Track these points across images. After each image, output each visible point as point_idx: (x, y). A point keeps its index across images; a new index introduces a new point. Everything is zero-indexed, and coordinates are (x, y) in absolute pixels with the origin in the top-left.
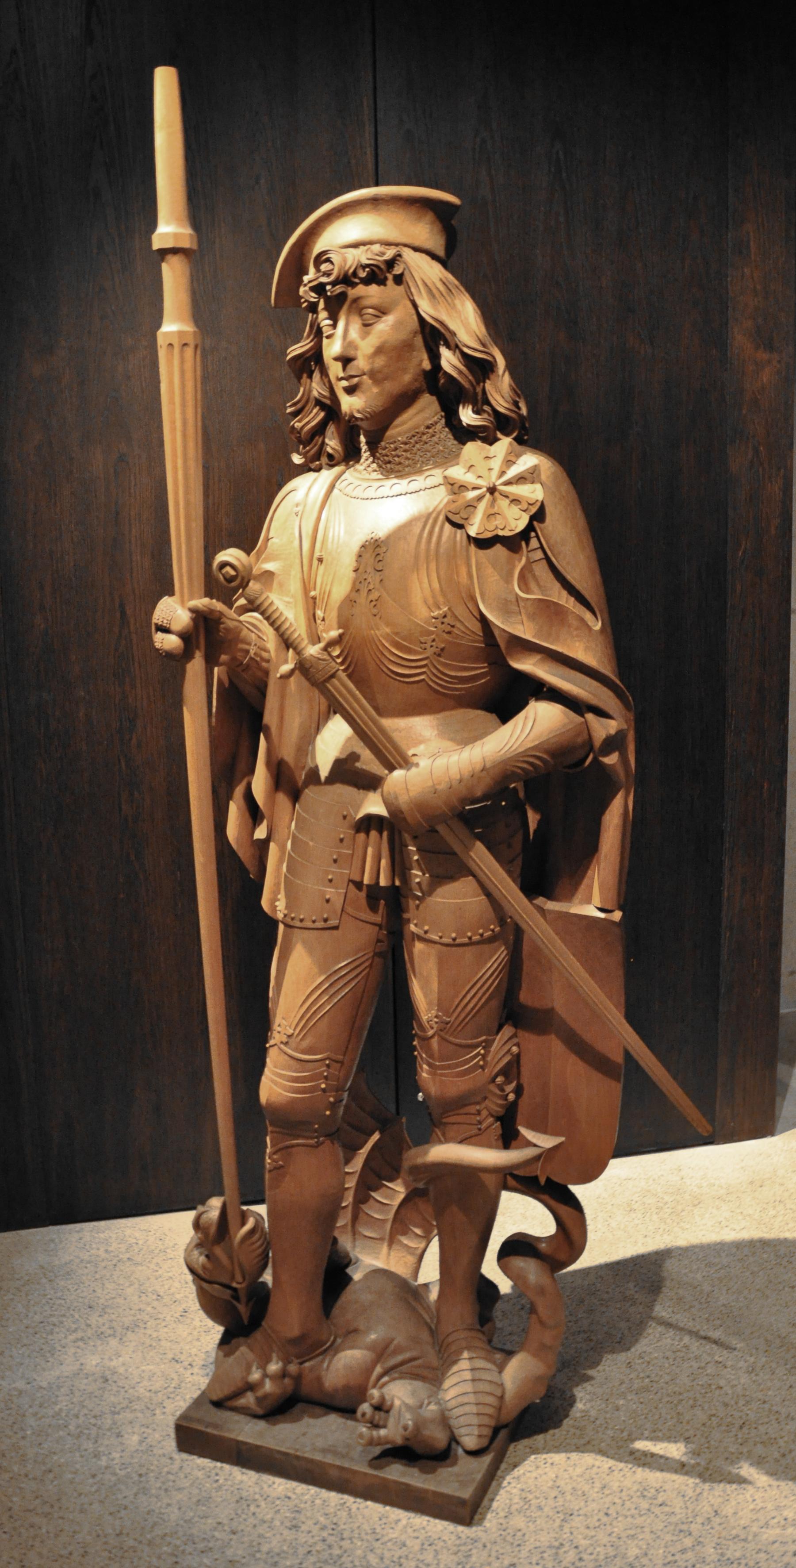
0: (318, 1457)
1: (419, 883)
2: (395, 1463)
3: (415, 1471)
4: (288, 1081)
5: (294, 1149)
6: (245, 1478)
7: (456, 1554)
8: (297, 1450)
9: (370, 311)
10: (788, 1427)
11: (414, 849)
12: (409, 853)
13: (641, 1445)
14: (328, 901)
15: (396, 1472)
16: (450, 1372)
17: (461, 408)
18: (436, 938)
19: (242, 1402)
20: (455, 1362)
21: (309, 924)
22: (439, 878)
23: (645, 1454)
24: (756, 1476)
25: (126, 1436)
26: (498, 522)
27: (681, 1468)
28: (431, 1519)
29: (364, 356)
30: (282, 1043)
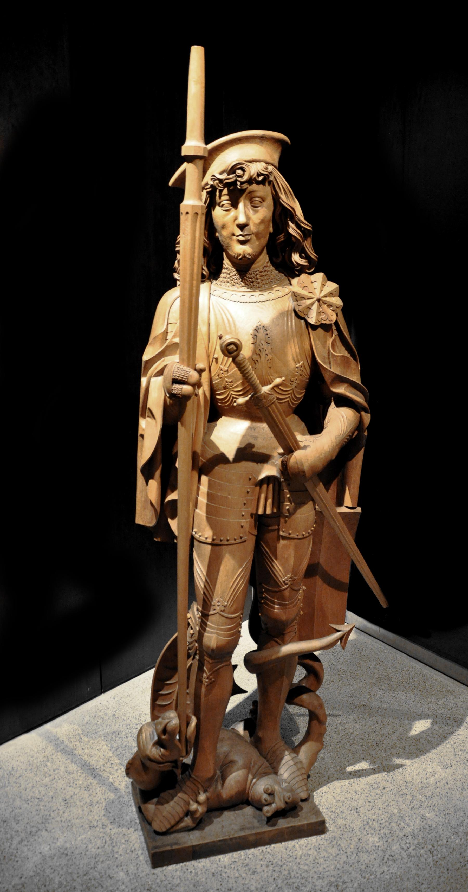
0: (242, 834)
1: (288, 510)
2: (279, 819)
3: (289, 819)
4: (225, 632)
5: (221, 669)
6: (203, 864)
7: (333, 847)
8: (229, 836)
9: (257, 199)
10: (393, 738)
11: (287, 491)
12: (284, 494)
13: (349, 769)
14: (242, 527)
15: (283, 823)
16: (282, 764)
17: (293, 255)
18: (295, 536)
19: (182, 825)
20: (282, 759)
21: (233, 542)
22: (299, 504)
23: (356, 772)
24: (404, 762)
25: (115, 876)
26: (323, 316)
27: (374, 771)
28: (307, 839)
29: (255, 224)
30: (221, 611)
